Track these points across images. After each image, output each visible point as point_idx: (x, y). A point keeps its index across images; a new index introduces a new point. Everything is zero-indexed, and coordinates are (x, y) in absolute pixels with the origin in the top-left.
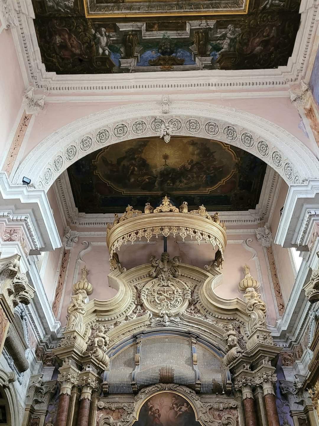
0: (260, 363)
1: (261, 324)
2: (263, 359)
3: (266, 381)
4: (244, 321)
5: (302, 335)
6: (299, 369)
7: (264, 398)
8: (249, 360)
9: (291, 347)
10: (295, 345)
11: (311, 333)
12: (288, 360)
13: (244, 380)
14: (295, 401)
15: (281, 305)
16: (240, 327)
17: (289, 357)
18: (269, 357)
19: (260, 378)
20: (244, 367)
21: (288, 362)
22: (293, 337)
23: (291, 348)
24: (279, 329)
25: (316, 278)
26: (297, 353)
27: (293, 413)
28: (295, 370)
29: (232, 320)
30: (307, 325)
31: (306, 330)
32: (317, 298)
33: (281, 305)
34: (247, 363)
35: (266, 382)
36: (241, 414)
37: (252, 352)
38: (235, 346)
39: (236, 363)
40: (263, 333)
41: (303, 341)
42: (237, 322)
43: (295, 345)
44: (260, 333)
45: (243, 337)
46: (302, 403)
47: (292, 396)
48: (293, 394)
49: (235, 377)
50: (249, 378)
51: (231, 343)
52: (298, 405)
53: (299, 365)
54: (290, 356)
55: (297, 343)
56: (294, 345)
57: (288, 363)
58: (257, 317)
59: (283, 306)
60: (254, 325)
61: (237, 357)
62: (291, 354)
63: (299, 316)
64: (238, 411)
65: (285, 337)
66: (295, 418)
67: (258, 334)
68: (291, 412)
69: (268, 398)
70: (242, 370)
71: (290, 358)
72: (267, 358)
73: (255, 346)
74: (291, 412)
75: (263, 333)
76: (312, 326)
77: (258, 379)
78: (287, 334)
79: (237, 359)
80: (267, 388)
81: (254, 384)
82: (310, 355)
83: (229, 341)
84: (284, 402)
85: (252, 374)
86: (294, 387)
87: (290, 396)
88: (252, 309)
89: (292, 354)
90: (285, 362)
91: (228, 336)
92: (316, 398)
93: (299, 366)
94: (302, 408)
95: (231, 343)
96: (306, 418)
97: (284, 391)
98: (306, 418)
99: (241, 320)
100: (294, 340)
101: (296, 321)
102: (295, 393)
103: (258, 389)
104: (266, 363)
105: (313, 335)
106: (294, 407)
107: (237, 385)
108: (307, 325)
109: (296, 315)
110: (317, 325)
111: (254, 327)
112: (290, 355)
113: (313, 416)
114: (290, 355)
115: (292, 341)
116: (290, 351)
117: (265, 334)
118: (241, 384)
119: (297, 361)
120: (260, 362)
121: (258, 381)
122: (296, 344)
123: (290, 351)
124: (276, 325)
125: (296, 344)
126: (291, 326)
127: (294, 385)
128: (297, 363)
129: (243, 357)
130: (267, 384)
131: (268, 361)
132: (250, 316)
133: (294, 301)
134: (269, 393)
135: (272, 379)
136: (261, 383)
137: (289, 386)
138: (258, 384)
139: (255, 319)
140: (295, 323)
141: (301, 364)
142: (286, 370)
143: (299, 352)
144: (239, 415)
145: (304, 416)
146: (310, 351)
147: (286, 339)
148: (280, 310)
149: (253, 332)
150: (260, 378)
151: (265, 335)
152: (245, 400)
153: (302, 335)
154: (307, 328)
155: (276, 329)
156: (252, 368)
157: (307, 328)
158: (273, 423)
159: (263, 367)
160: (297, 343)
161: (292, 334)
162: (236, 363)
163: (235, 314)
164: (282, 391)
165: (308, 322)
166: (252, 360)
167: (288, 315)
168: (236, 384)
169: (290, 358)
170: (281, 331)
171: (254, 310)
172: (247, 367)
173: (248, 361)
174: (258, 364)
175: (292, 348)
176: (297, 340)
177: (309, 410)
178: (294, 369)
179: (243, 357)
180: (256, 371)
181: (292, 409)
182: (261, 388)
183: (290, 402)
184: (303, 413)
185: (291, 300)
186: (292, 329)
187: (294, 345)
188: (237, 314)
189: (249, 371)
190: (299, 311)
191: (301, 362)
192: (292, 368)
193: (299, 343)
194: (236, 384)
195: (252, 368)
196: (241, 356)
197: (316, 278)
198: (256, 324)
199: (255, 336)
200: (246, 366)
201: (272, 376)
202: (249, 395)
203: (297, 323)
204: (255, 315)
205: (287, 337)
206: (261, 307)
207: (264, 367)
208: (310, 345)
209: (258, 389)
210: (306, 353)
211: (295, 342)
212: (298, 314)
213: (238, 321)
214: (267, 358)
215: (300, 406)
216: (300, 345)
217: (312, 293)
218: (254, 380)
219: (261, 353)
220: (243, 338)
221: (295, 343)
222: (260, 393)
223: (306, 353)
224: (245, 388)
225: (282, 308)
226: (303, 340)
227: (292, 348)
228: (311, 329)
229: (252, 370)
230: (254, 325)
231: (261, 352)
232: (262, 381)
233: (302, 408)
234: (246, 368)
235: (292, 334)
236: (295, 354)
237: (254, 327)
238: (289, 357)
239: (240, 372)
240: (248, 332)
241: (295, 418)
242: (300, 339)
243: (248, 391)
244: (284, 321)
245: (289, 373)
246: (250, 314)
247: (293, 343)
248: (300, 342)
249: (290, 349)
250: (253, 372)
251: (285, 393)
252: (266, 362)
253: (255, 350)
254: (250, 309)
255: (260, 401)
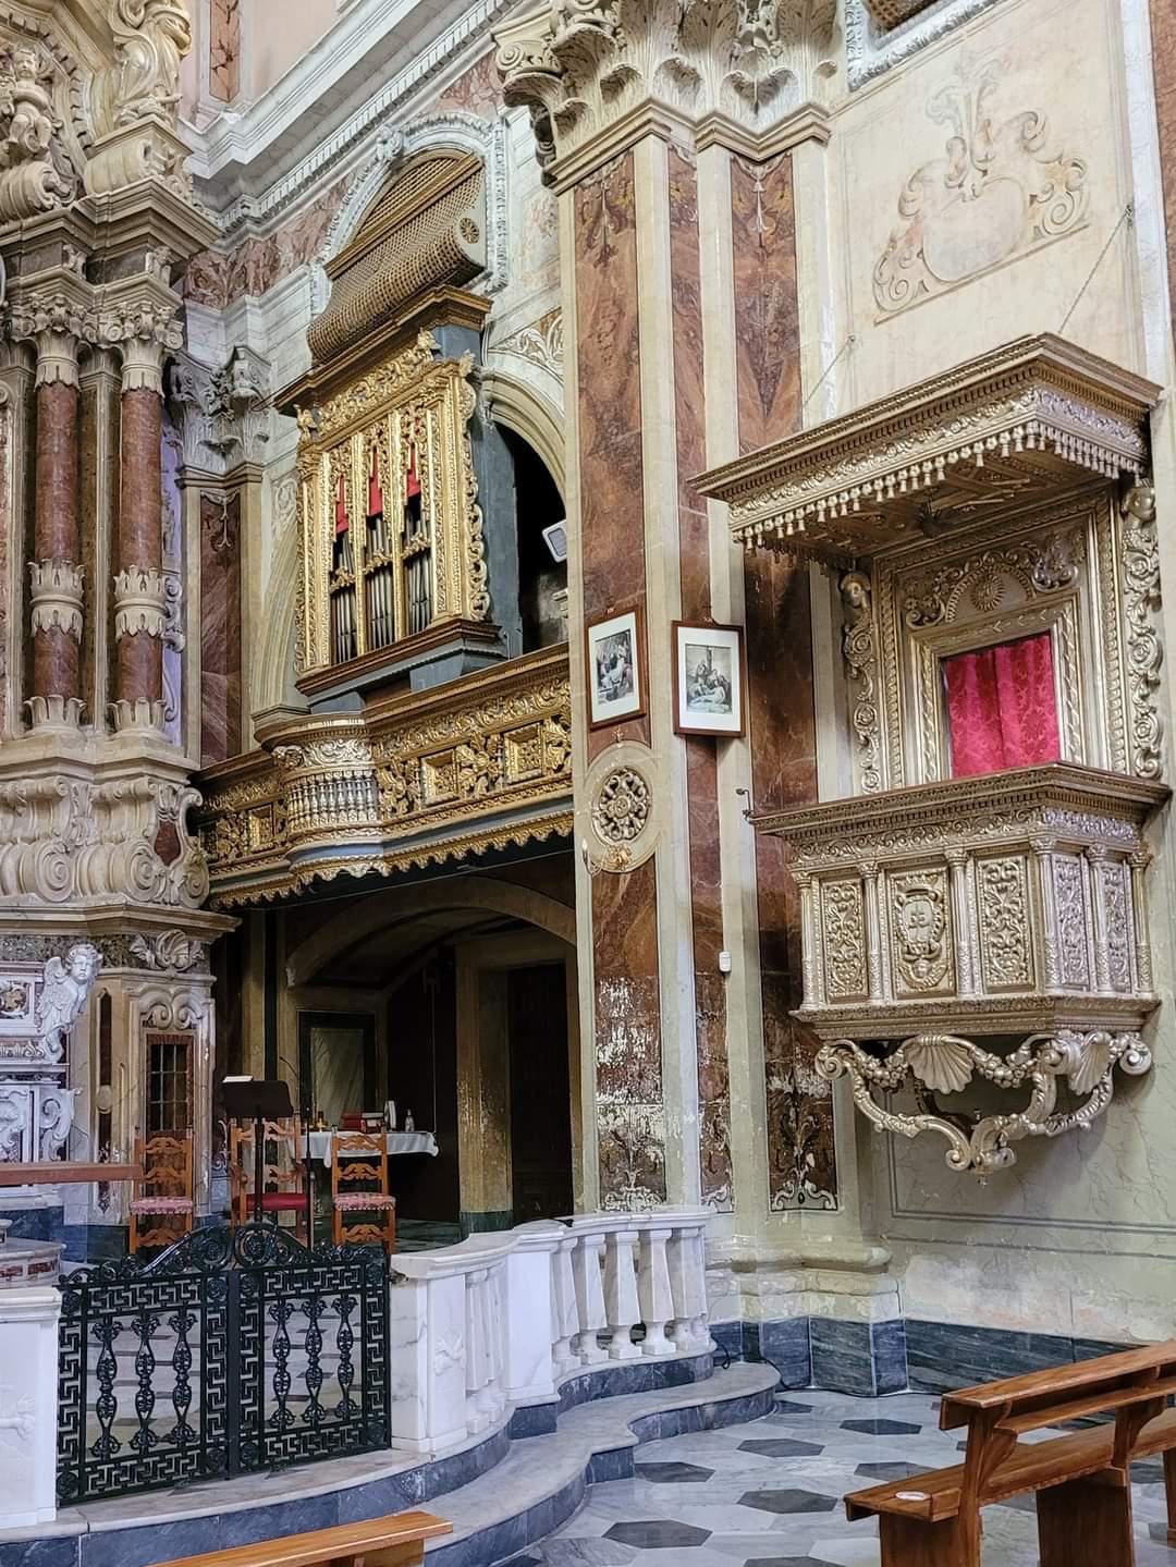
0: (128, 261)
1: (163, 104)
2: (149, 250)
3: (145, 338)
4: (78, 60)
5: (299, 207)
6: (247, 330)
7: (119, 399)
8: (89, 236)
9: (234, 237)
10: (251, 235)
11: (348, 208)
12: (207, 279)
13: (60, 311)
14: (202, 439)
15: (222, 47)
16: (56, 80)
17: (211, 272)
18: (171, 250)
19: (123, 320)
20: (65, 257)
21: (208, 292)
22: (257, 201)
23: (230, 240)
24: (216, 150)
25: (583, 12)
26: (251, 266)
27: (189, 475)
28: (227, 326)
29: (30, 33)
30: (337, 175)
31: (324, 192)
32: (535, 93)
33: (222, 47)
34: (82, 246)
35: (144, 342)
36: (18, 433)
37: (111, 207)
38: (37, 156)
39: (29, 229)
40: (166, 144)
41: (291, 230)
42: (48, 55)
43: (251, 235)
44: (155, 139)
45: (62, 128)
46: (224, 449)
47: (200, 418)
48: (205, 411)
49: (18, 287)
50: (78, 307)
51: (26, 139)
52: (209, 452)
53: (252, 314)
54: (217, 271)
55: (260, 229)
56: (247, 231)
57: (204, 295)
58: (155, 69)
59: (230, 58)
60: (136, 97)
61: (43, 209)
62: (223, 265)
63: (323, 128)
64: (10, 422)
65: (226, 189)
66: (193, 493)
67: (150, 143)
68: (181, 469)
69: (137, 400)
70: (57, 269)
71: (215, 277)
72: (163, 253)
73: (135, 190)
74: (181, 469)
75: (166, 144)
76: (362, 185)
77: (110, 322)
78: (241, 184)
79: (42, 216)
80: (142, 365)
81: (91, 336)
82: (315, 291)
83: (19, 126)
84: (166, 430)
85: (90, 294)
86: (212, 388)
87: (191, 415)
88: (137, 20)
89: (224, 266)
90: (197, 286)
91: (17, 102)
92: (318, 444)
93: (249, 315)
94: (220, 466)
95: (26, 139)
96: (225, 504)
97: (179, 391)
98: (225, 504)
99: (67, 49)
100: (255, 213)
101: (300, 140)
102: (212, 409)
103: (103, 358)
104: (153, 265)
105: (354, 222)
106: (198, 458)
107: (22, 322)
108: (337, 175)
109: (316, 117)
110: (386, 189)
111: (133, 104)
112: (216, 266)
113: (257, 502)
114: (216, 266)
115: (246, 216)
116: (220, 251)
117: (172, 151)
118: (44, 321)
119: (248, 298)
120: (133, 259)
121: (109, 331)
122: (257, 234)
123: (220, 251)
124: (212, 129)
125: (257, 234)
126: (273, 158)
127: (214, 383)
128: (245, 304)
129: (72, 217)
130: (146, 350)
131: (163, 266)
132: (121, 47)
133: (336, 57)
134: (146, 384)
135: (165, 336)
136: (125, 342)
137: (198, 379)
138: (109, 342)
139: (143, 71)
140: (290, 150)
141: (260, 312)
142: (199, 319)
143: (258, 267)
144: (10, 437)
145: (222, 497)
146: (320, 275)
147: (225, 199)
148: (215, 69)
149: (124, 124)
150: (123, 320)
151: (170, 157)
152: (49, 391)
153: (299, 207)
154: (330, 187)
155: (204, 146)
156: (92, 271)
157: (330, 187)
158: (143, 495)
159: (146, 282)
160: (260, 229)
161: (260, 186)
162: (29, 229)
163: (50, 10)
164: (174, 389)
165: (349, 164)
166: (99, 238)
167: (283, 107)
168: (18, 317)
169: (215, 277)
170: (224, 161)
171: (144, 28)
172: (76, 263)
173: (84, 238)
174: (118, 261)
175: (234, 242)
176: (266, 217)
177: (250, 478)
178: (222, 324)
179: (72, 217)
180: (108, 287)
181: (189, 461)
182: (117, 359)
183: (187, 435)
184: (220, 485)
185: (327, 49)
186: (267, 169)
187: (247, 231)
188: (55, 16)
189: (80, 277)
190: (336, 107)
191: (261, 307)
192: (219, 319)
193: (268, 231)
194: (18, 317)
195: (92, 271)
196: (59, 208)
197: (583, 12)
198: (142, 95)
199: (137, 145)
200: (73, 258)
201: (166, 325)
202: (68, 375)
203: (299, 150)
204: (147, 52)
205: (233, 191)
206: (177, 27)
207: (152, 285)
208: (329, 253)
209: (103, 358)
210: (300, 278)
211: (257, 222)
212: (324, 116)
213: (52, 49)
214: (163, 253)
215: (217, 458)
216: (274, 240)
217: (526, 64)
218: (95, 324)
219: (149, 222)
220: (60, 133)
221: (255, 228)
222: (104, 378)
223: (300, 278)
224: (55, 342)
225: (223, 66)
226: (296, 226)
227: (234, 242)
228: (355, 196)
229: (91, 279)
230: (136, 97)
231: (152, 219)
232: (128, 335)
233: (220, 466)
234: (71, 265)
235: (260, 186)
236: (238, 269)
237: (133, 104)
238: (214, 274)
239: (49, 272)
240: (87, 117)
241: (193, 493)
242: (283, 219)
243: (64, 355)
244: (251, 123)
245: (206, 331)
246: (122, 40)
247: (249, 224)
248: (277, 230)
249: (224, 243)
250: (96, 289)
251: (183, 402)
252: (157, 266)
253: (132, 203)
254: (129, 16)
255: (102, 405)
